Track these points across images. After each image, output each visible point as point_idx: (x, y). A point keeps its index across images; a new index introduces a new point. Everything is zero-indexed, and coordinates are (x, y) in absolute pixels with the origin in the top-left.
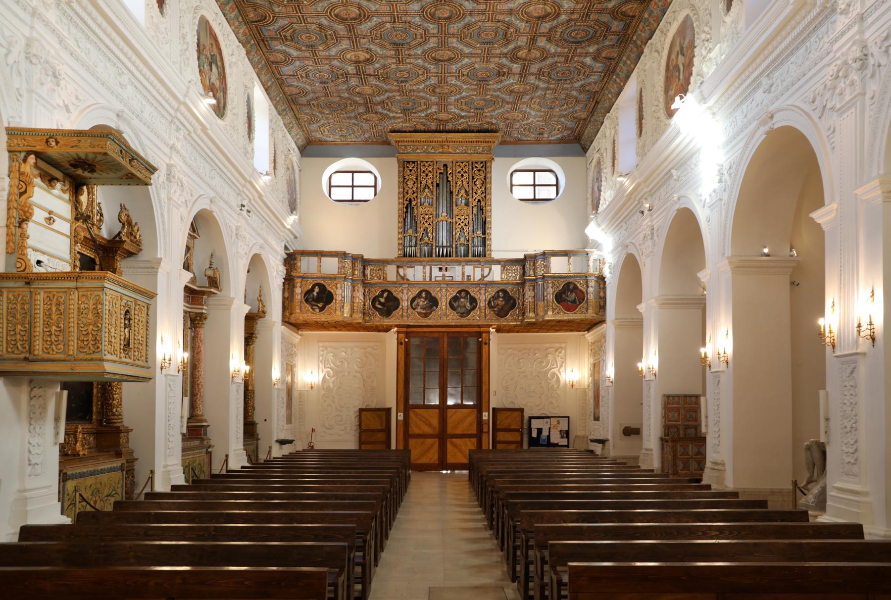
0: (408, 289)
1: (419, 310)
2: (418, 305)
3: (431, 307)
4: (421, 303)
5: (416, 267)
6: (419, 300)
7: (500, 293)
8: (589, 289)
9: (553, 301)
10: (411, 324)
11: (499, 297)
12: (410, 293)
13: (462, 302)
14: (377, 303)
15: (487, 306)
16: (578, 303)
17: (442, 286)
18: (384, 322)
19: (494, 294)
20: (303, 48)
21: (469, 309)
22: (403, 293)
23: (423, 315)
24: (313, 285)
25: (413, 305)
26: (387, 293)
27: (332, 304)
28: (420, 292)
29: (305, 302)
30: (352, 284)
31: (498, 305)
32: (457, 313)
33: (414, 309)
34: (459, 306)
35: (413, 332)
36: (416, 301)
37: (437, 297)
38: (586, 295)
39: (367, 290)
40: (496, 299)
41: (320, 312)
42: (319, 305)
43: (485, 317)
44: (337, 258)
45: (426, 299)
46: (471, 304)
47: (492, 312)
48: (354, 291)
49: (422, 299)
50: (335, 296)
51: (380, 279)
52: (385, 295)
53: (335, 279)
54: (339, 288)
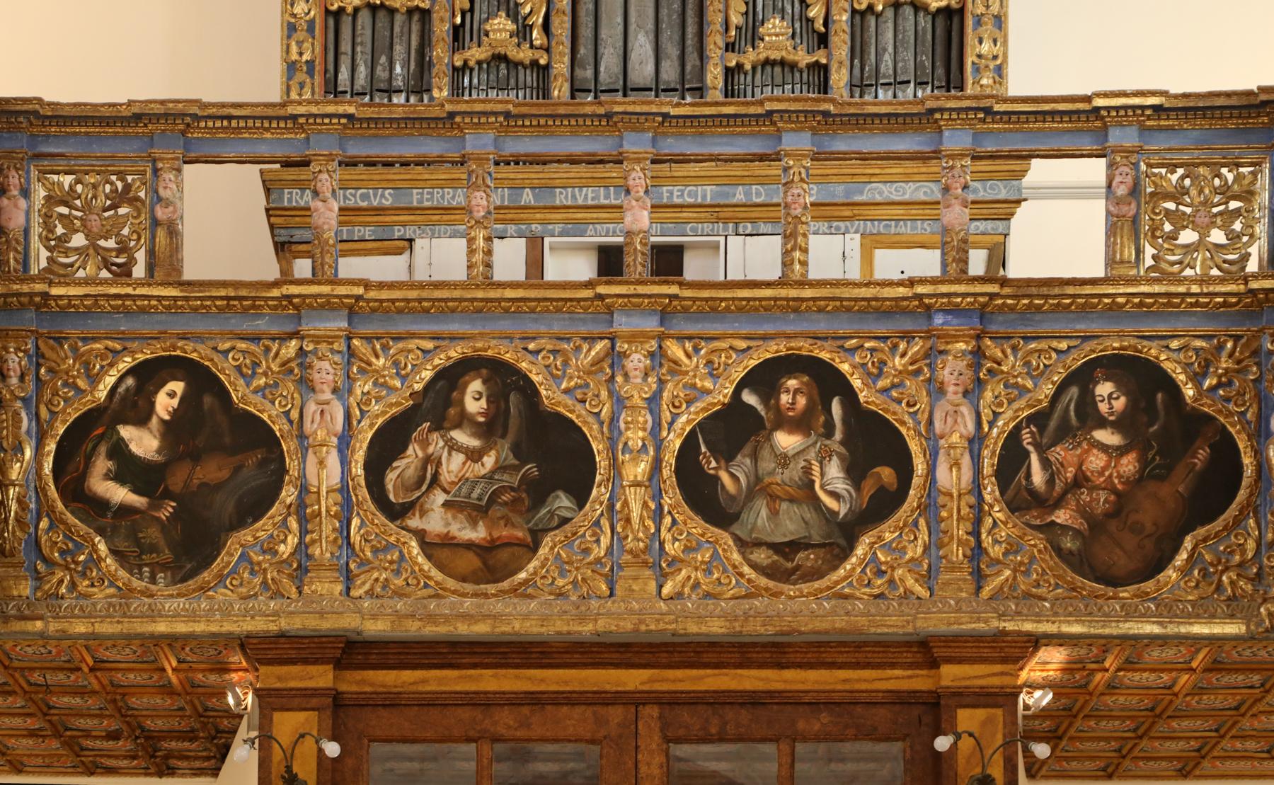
0: (351, 353)
1: (436, 520)
2: (429, 478)
3: (538, 492)
4: (453, 466)
5: (418, 244)
6: (437, 444)
7: (1104, 389)
10: (376, 628)
11: (1089, 416)
12: (363, 386)
13: (784, 460)
14: (102, 464)
15: (991, 491)
17: (623, 324)
18: (154, 614)
19: (1048, 389)
21: (842, 509)
22: (307, 385)
23: (470, 561)
25: (391, 477)
26: (178, 386)
28: (441, 375)
31: (1081, 480)
32: (742, 544)
33: (396, 512)
34: (758, 487)
35: (392, 701)
36: (414, 452)
37: (577, 414)
40: (1064, 433)
43: (979, 578)
45: (490, 429)
46: (855, 473)
49: (461, 436)
51: (124, 272)
52: (166, 401)
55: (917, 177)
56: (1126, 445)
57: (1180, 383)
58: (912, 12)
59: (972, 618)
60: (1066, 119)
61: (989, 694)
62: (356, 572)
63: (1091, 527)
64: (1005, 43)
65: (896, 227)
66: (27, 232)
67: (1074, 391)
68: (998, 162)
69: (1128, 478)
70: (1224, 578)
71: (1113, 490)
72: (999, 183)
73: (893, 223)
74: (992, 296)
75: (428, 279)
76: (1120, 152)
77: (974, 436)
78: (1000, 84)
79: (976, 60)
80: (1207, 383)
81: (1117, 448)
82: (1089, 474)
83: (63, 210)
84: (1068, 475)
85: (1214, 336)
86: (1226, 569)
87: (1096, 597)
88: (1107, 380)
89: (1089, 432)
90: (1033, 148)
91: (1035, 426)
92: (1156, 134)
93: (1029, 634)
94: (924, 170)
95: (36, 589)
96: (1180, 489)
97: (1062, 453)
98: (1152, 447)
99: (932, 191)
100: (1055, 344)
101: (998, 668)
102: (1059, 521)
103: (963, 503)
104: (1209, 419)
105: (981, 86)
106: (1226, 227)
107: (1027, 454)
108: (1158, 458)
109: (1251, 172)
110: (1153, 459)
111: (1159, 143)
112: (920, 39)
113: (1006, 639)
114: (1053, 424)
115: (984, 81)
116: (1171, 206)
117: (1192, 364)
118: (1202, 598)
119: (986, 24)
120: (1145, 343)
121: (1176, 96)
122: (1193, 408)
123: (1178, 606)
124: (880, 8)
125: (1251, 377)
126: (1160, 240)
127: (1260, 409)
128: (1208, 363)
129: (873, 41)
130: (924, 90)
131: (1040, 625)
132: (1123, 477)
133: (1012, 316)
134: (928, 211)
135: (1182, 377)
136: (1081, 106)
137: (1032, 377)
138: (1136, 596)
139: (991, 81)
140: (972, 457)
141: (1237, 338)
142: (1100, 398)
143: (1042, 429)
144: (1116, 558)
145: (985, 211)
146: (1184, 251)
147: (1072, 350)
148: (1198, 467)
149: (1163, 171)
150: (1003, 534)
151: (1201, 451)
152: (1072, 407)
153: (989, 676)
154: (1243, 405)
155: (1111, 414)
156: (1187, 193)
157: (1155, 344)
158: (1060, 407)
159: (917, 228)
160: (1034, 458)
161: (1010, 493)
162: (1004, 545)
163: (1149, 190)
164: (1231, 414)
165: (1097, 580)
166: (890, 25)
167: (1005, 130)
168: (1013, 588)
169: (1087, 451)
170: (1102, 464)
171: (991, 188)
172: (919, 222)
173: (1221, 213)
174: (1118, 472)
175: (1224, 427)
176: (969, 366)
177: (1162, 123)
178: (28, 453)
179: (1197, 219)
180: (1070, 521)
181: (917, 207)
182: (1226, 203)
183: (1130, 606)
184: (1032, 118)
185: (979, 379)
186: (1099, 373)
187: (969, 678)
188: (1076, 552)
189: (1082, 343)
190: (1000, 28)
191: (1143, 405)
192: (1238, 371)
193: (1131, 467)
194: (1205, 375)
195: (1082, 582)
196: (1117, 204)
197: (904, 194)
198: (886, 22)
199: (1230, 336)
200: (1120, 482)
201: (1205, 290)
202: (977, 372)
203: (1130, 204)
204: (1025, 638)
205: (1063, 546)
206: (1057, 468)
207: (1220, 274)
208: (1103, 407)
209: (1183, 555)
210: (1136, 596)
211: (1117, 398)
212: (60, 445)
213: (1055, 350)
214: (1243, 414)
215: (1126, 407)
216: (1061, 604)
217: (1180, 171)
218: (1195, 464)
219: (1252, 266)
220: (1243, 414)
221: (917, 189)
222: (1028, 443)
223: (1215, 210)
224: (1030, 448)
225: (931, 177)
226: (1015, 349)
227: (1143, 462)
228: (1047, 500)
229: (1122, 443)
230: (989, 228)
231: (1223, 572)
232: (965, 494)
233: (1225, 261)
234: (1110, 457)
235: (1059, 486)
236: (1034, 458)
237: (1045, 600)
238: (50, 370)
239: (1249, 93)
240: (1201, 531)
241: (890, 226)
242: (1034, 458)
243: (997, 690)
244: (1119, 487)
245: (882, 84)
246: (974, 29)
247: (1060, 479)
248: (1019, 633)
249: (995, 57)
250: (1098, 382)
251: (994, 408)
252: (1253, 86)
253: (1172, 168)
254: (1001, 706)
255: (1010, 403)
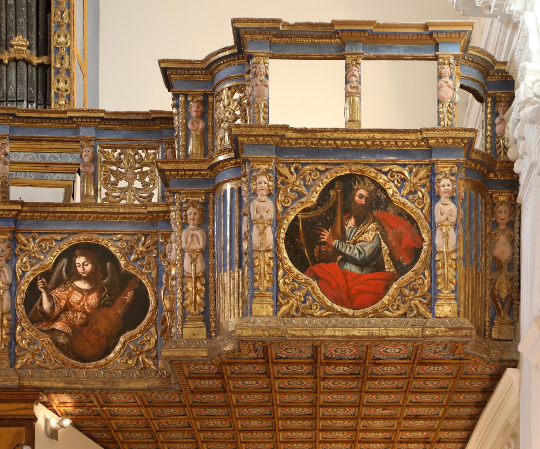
7: (80, 260)
8: (438, 206)
9: (277, 258)
15: (21, 310)
16: (389, 267)
19: (51, 260)
20: (491, 287)
31: (68, 307)
38: (425, 236)
40: (60, 282)
47: (47, 338)
55: (25, 150)
56: (91, 289)
57: (118, 258)
58: (25, 65)
59: (4, 379)
60: (57, 122)
61: (17, 420)
62: (18, 354)
63: (73, 332)
64: (71, 83)
65: (16, 175)
67: (65, 261)
68: (65, 144)
69: (92, 306)
70: (140, 358)
71: (85, 312)
72: (68, 154)
73: (14, 173)
74: (19, 211)
75: (19, 200)
76: (84, 140)
77: (12, 283)
78: (69, 104)
79: (56, 91)
80: (133, 257)
81: (87, 291)
82: (72, 304)
84: (62, 304)
85: (136, 234)
86: (141, 353)
87: (75, 368)
88: (82, 255)
89: (73, 282)
90: (41, 136)
91: (45, 278)
92: (105, 132)
93: (36, 388)
94: (27, 146)
96: (118, 312)
97: (59, 293)
98: (104, 290)
99: (34, 157)
100: (54, 236)
101: (23, 405)
102: (57, 328)
103: (5, 318)
104: (133, 276)
105: (59, 105)
106: (141, 180)
107: (40, 293)
108: (107, 296)
109: (154, 153)
110: (105, 296)
111: (107, 136)
112: (29, 79)
113: (24, 390)
114: (54, 278)
115: (61, 103)
116: (114, 168)
117: (125, 248)
118: (129, 369)
119: (62, 73)
120: (101, 237)
121: (111, 113)
122: (125, 271)
123: (115, 373)
124: (6, 61)
125: (154, 255)
126: (109, 185)
127: (158, 271)
128: (132, 248)
129: (5, 78)
130: (32, 105)
131: (42, 383)
132: (89, 305)
133: (32, 222)
134: (32, 168)
135: (119, 255)
136: (63, 116)
137: (43, 253)
138: (95, 367)
139: (64, 102)
140: (11, 294)
141: (146, 236)
142: (78, 265)
143: (48, 280)
144: (86, 348)
145: (61, 169)
146: (120, 191)
147: (64, 240)
148: (127, 301)
149: (110, 150)
150: (27, 334)
151: (129, 293)
152: (64, 269)
153: (18, 409)
154: (150, 269)
155: (84, 273)
156: (122, 162)
157: (106, 238)
158: (57, 269)
159: (27, 176)
160: (44, 295)
161: (32, 313)
162: (27, 341)
163: (103, 159)
164: (143, 274)
165: (76, 359)
166: (13, 71)
167: (25, 127)
168: (33, 363)
169: (71, 292)
170: (79, 299)
171: (64, 157)
172: (28, 173)
173: (138, 173)
174: (87, 303)
175: (141, 281)
176: (9, 246)
177: (107, 126)
179: (127, 175)
180: (62, 328)
181: (26, 165)
182: (142, 168)
183: (91, 373)
184: (39, 121)
185: (15, 253)
186: (78, 252)
187: (7, 411)
188: (65, 344)
189: (68, 236)
190: (69, 76)
191: (100, 269)
192: (147, 252)
193: (94, 300)
194: (131, 254)
195: (67, 360)
196: (84, 166)
197: (19, 158)
198: (11, 69)
199: (143, 234)
200: (88, 308)
201: (127, 211)
202: (13, 250)
203: (91, 166)
204: (34, 390)
205: (59, 341)
206: (56, 301)
207: (139, 203)
208: (80, 269)
209: (118, 347)
210: (95, 367)
211: (87, 265)
213: (55, 240)
214: (150, 273)
215: (92, 269)
216: (55, 372)
217: (119, 151)
218: (126, 299)
219: (155, 200)
220: (150, 273)
221: (25, 156)
222: (41, 288)
223: (136, 171)
224: (42, 290)
225: (32, 150)
226: (34, 239)
227: (100, 298)
228: (51, 317)
229: (89, 288)
230: (65, 177)
231: (139, 355)
232: (6, 313)
233: (141, 197)
234: (83, 295)
235: (57, 310)
236: (44, 295)
237: (48, 369)
239: (146, 113)
240: (128, 334)
241: (13, 174)
242: (44, 295)
243: (21, 417)
244: (88, 311)
245: (9, 101)
246: (56, 75)
247: (57, 306)
248: (31, 387)
249: (66, 90)
250: (77, 257)
251: (23, 269)
252: (148, 110)
253: (115, 149)
254: (24, 426)
255: (31, 267)
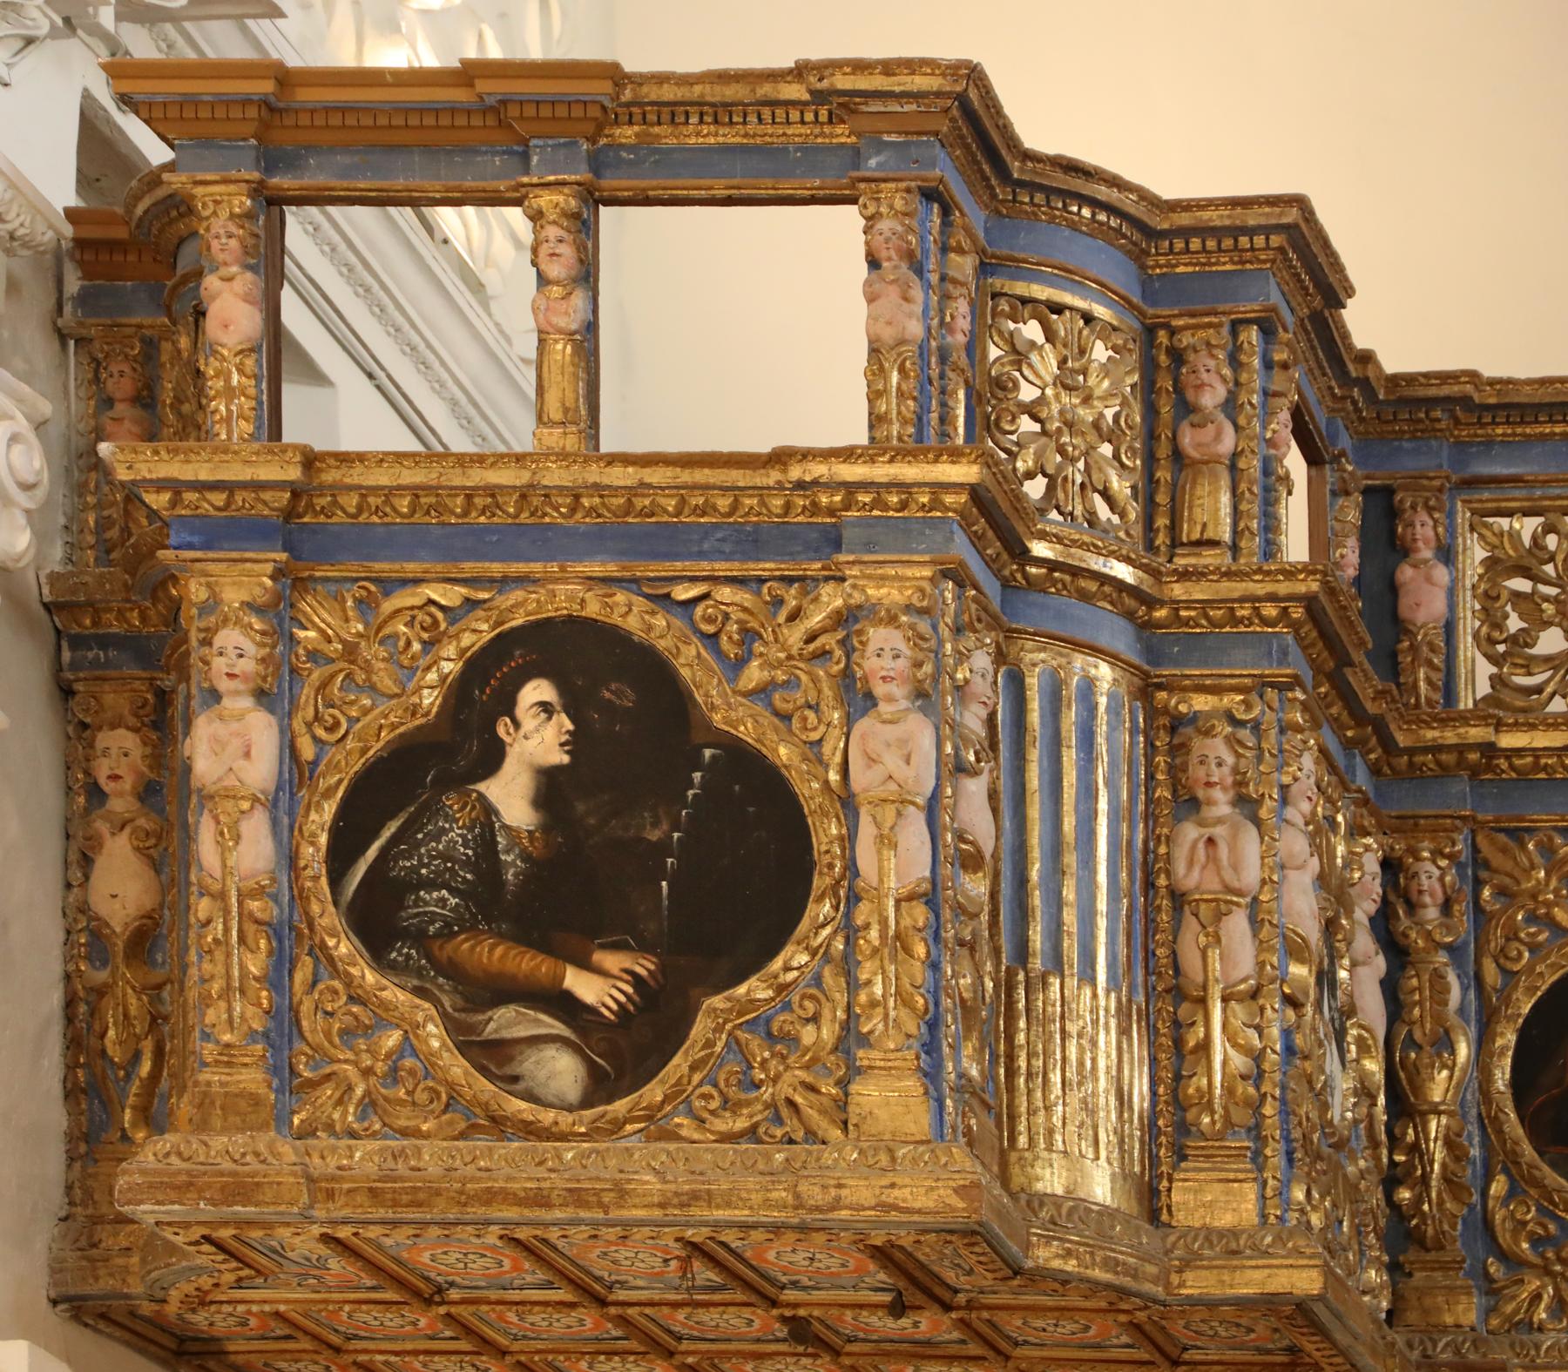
24: (478, 666)
27: (794, 956)
29: (344, 947)
30: (1145, 689)
39: (1431, 876)
41: (600, 1087)
42: (584, 987)
44: (848, 218)
48: (1189, 804)
50: (826, 832)
53: (833, 540)
54: (893, 695)
66: (1450, 628)
83: (1521, 585)
95: (1489, 1312)
178: (1463, 1051)
212: (1523, 1034)
238: (1501, 892)
